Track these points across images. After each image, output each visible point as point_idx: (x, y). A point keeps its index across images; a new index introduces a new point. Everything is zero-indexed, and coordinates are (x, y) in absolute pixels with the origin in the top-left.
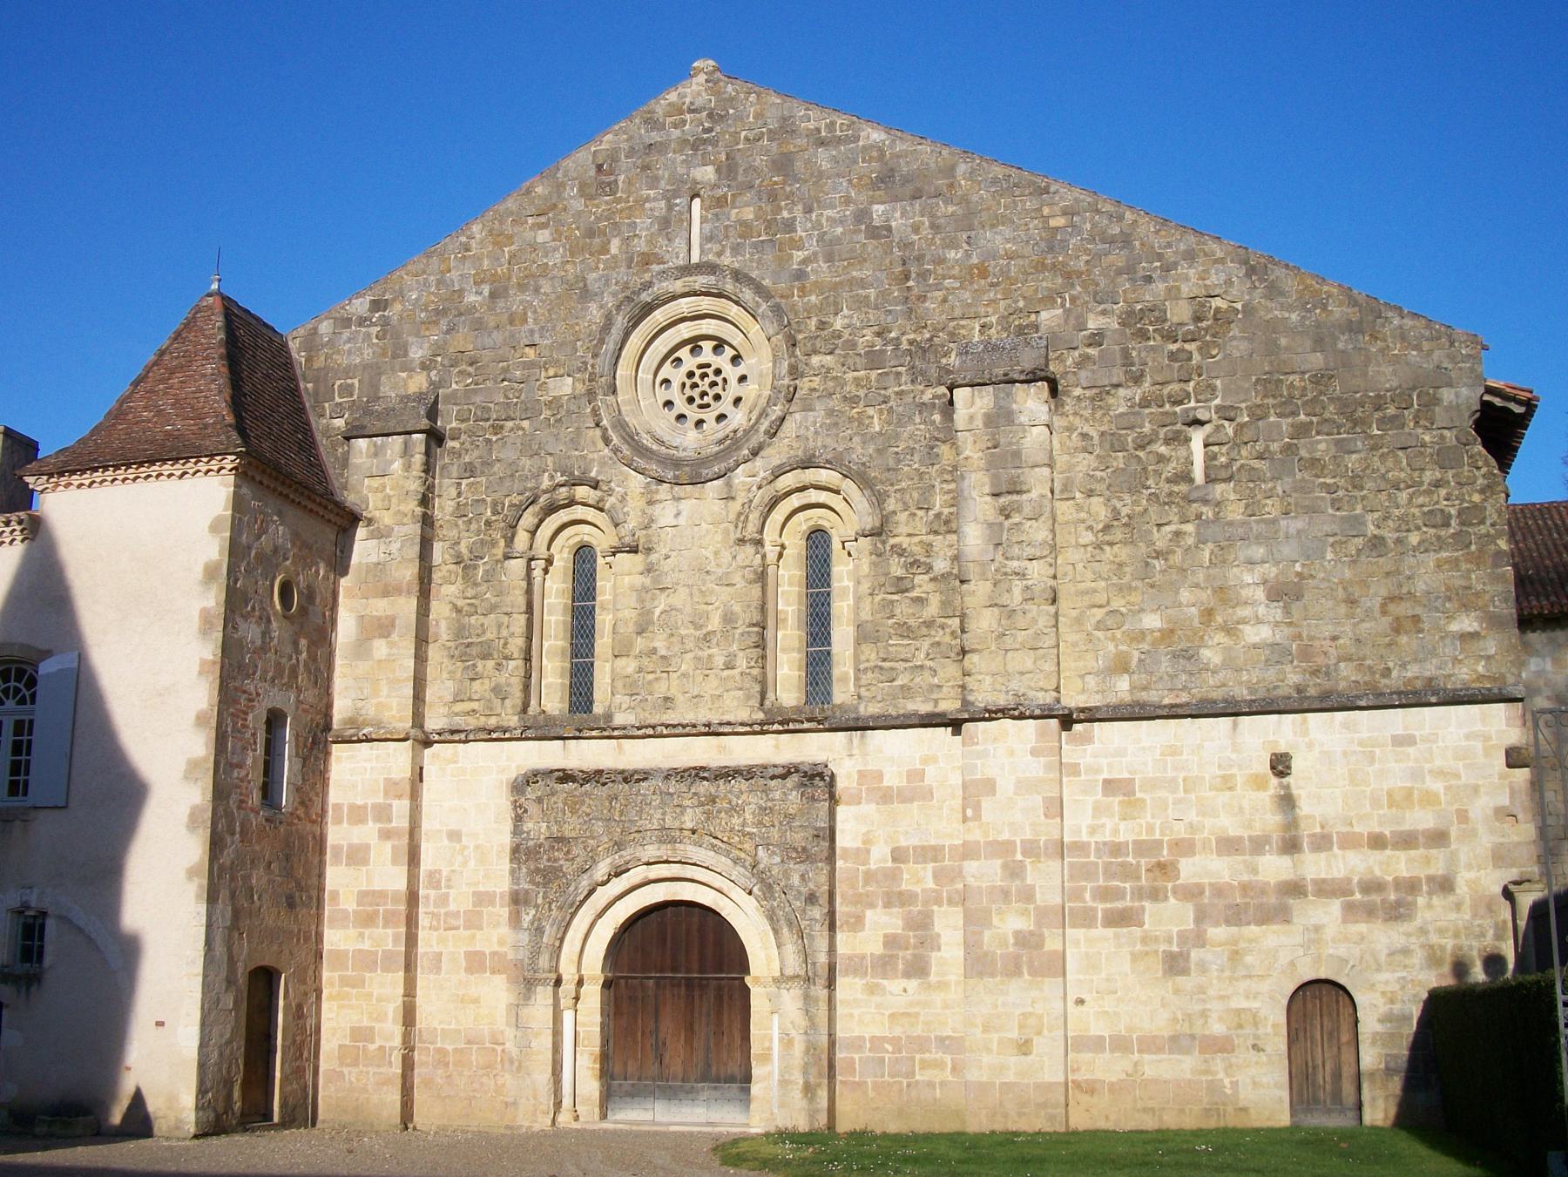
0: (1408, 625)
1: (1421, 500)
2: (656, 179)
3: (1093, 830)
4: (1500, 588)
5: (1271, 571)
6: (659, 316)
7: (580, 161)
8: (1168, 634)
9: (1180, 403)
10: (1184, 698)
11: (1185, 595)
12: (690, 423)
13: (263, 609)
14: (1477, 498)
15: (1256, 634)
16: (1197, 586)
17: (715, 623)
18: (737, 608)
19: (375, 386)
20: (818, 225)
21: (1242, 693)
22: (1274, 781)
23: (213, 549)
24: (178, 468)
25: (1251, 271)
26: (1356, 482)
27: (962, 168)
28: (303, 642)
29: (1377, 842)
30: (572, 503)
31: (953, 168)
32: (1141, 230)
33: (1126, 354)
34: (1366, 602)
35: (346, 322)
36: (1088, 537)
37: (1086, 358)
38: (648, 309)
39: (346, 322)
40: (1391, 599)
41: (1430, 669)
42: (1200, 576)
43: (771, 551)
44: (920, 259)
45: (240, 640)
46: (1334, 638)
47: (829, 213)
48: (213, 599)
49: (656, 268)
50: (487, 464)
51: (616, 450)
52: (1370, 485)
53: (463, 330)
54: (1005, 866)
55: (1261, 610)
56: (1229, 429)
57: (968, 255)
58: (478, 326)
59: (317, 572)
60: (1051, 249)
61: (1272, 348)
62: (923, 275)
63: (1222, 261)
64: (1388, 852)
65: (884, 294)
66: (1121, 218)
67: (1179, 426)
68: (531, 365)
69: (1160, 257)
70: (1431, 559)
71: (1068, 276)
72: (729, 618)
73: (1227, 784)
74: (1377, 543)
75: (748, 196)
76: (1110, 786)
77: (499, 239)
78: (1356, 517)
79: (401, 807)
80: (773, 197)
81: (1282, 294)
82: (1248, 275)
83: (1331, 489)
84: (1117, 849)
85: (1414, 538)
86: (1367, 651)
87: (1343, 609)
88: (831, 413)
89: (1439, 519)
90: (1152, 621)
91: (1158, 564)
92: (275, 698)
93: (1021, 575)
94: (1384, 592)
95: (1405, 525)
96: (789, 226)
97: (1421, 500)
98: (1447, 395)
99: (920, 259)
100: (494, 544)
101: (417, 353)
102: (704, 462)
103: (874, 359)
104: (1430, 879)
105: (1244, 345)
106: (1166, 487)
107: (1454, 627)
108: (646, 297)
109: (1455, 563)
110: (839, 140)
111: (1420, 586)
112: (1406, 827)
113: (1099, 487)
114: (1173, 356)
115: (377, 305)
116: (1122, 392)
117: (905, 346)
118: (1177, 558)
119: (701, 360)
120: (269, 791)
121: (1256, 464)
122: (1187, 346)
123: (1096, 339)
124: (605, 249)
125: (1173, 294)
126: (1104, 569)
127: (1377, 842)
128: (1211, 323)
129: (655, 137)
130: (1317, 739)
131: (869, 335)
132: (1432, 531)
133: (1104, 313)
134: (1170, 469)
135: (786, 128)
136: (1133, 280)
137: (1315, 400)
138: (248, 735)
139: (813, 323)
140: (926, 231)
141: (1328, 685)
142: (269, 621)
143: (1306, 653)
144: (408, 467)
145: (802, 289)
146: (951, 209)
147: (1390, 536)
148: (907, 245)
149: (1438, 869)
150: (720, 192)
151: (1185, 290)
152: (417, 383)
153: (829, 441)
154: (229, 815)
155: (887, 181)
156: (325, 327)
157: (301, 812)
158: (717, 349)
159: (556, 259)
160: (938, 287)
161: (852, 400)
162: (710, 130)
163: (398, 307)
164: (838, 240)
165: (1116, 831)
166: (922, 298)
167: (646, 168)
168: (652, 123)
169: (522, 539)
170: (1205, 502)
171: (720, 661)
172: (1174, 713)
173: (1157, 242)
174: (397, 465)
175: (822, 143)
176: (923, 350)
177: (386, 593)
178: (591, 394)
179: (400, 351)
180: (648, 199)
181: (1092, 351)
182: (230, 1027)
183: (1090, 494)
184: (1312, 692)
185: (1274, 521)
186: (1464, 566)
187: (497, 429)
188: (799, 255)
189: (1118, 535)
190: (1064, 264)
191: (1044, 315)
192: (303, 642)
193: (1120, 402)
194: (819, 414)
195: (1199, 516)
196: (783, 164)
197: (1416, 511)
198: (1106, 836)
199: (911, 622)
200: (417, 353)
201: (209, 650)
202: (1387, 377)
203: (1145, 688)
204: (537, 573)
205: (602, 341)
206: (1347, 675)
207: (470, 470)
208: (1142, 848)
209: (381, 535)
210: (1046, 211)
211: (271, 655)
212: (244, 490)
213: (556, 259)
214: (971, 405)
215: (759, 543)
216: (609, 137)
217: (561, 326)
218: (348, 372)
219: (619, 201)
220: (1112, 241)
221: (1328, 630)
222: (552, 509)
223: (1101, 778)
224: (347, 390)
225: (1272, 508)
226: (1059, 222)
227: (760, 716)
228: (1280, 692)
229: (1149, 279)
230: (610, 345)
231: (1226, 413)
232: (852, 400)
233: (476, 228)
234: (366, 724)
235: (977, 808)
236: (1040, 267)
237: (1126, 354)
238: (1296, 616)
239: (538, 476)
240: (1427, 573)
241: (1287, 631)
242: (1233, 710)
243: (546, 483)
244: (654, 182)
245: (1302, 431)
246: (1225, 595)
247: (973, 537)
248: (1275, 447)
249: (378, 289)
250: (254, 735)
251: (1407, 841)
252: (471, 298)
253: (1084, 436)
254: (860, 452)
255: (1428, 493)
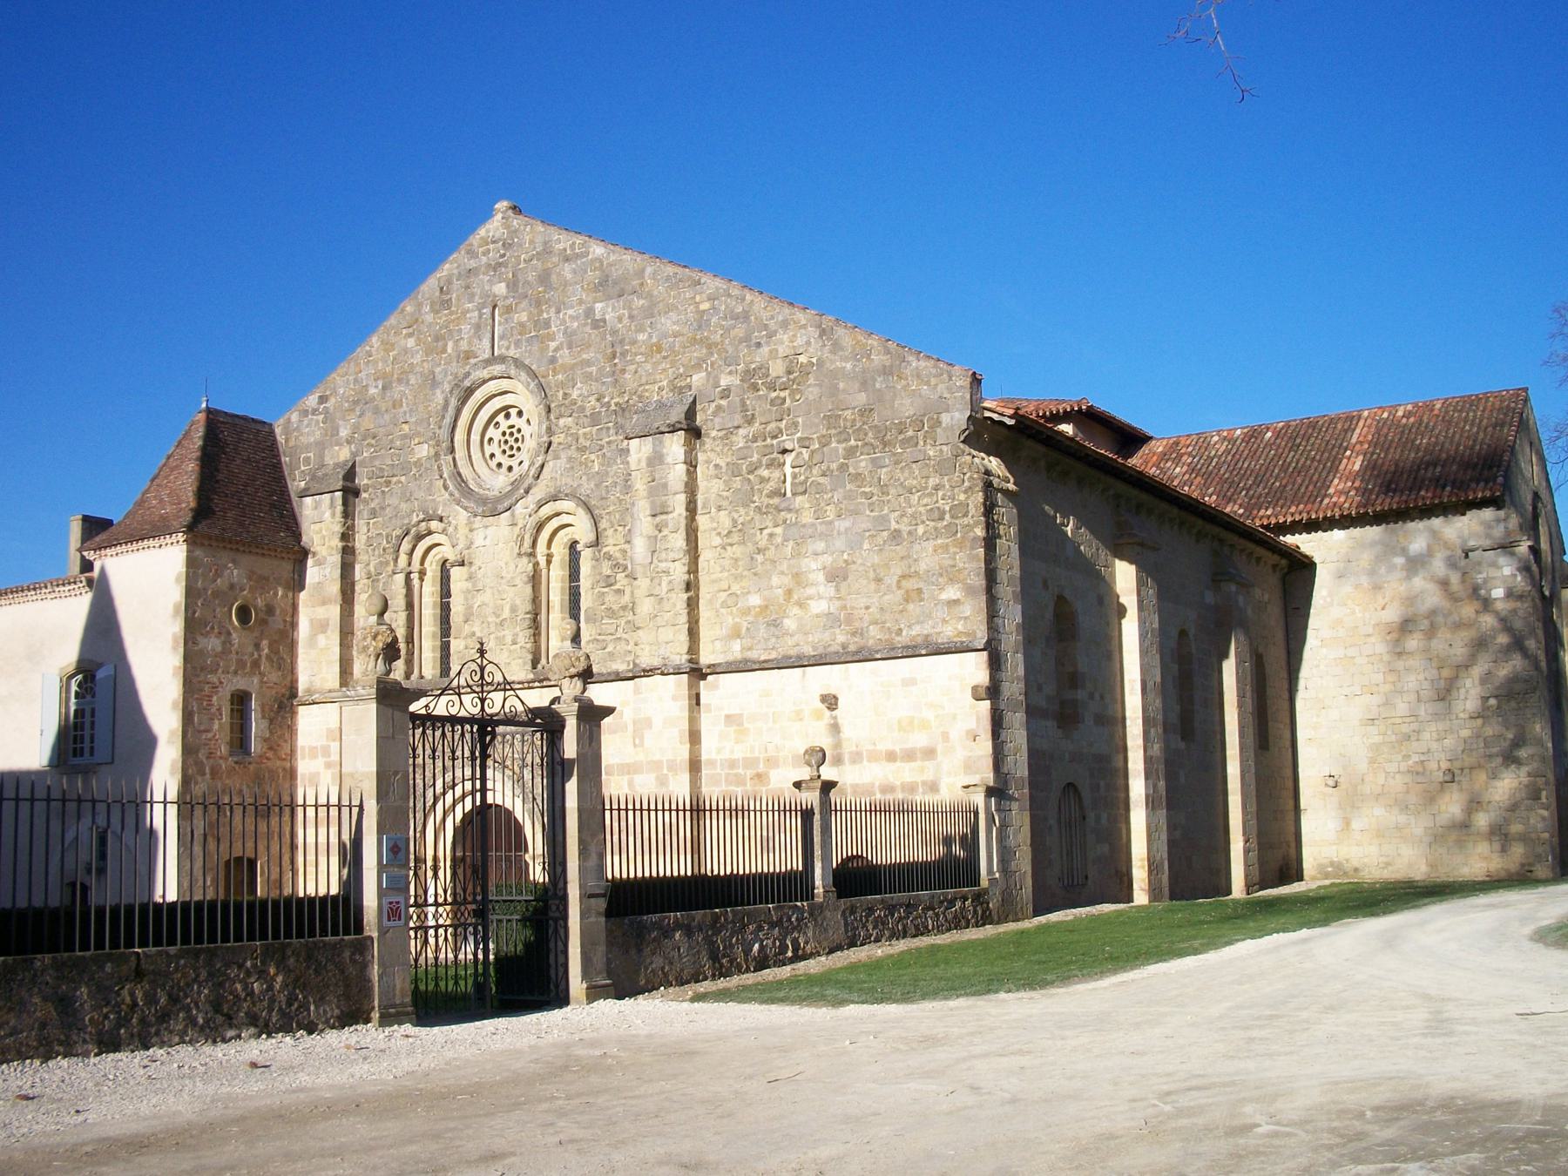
0: (914, 595)
1: (925, 501)
2: (473, 295)
3: (719, 751)
4: (974, 565)
5: (827, 560)
6: (479, 395)
7: (430, 285)
8: (764, 608)
9: (775, 437)
10: (773, 655)
11: (775, 580)
12: (504, 469)
13: (221, 626)
14: (962, 497)
15: (819, 607)
16: (782, 573)
17: (506, 613)
18: (518, 602)
19: (322, 457)
20: (563, 322)
21: (808, 650)
22: (827, 713)
23: (176, 594)
24: (156, 542)
25: (823, 332)
26: (884, 490)
27: (649, 270)
28: (265, 643)
29: (891, 757)
30: (430, 533)
31: (643, 271)
32: (755, 308)
33: (743, 403)
34: (887, 580)
35: (305, 413)
36: (717, 541)
37: (719, 408)
38: (470, 392)
39: (305, 413)
40: (903, 577)
41: (927, 629)
42: (784, 567)
43: (542, 561)
44: (622, 342)
45: (201, 651)
46: (867, 608)
47: (570, 312)
48: (177, 627)
49: (473, 361)
50: (383, 508)
51: (451, 495)
52: (893, 491)
53: (369, 414)
54: (657, 778)
55: (822, 589)
56: (806, 454)
57: (650, 337)
58: (377, 411)
59: (276, 594)
60: (700, 327)
61: (834, 391)
62: (624, 354)
63: (804, 327)
64: (898, 764)
65: (600, 370)
66: (743, 299)
67: (775, 455)
68: (405, 437)
69: (766, 327)
70: (929, 546)
71: (709, 347)
72: (513, 609)
73: (799, 716)
74: (896, 535)
75: (524, 304)
76: (729, 719)
77: (388, 346)
78: (883, 517)
79: (335, 746)
80: (538, 303)
81: (842, 349)
82: (820, 336)
83: (869, 496)
84: (732, 764)
85: (921, 529)
86: (887, 616)
87: (873, 586)
88: (570, 459)
89: (936, 515)
90: (755, 600)
91: (760, 558)
92: (240, 683)
93: (667, 572)
94: (899, 572)
95: (915, 519)
96: (547, 324)
97: (925, 501)
98: (945, 418)
99: (622, 342)
100: (387, 563)
101: (344, 433)
102: (499, 500)
103: (595, 419)
104: (924, 783)
105: (816, 390)
106: (766, 501)
107: (944, 596)
108: (467, 383)
109: (945, 547)
110: (578, 256)
111: (923, 566)
112: (909, 745)
113: (725, 503)
114: (772, 402)
115: (323, 399)
116: (741, 432)
117: (613, 407)
118: (771, 553)
119: (510, 422)
120: (240, 741)
121: (822, 480)
122: (782, 394)
123: (726, 393)
124: (444, 351)
125: (773, 354)
126: (727, 563)
127: (891, 757)
128: (796, 374)
129: (473, 264)
130: (853, 682)
131: (592, 399)
132: (932, 524)
133: (730, 373)
134: (771, 486)
135: (547, 251)
136: (749, 347)
137: (859, 429)
138: (214, 710)
139: (560, 394)
140: (626, 321)
141: (862, 642)
142: (229, 634)
143: (849, 619)
144: (333, 515)
145: (554, 370)
146: (642, 302)
147: (904, 528)
148: (614, 332)
149: (929, 776)
150: (508, 302)
151: (781, 352)
152: (344, 454)
153: (569, 481)
154: (200, 766)
155: (608, 286)
156: (295, 417)
157: (270, 754)
158: (508, 416)
159: (417, 359)
160: (632, 362)
161: (582, 450)
162: (503, 256)
163: (332, 400)
164: (574, 333)
165: (732, 752)
166: (623, 371)
167: (467, 287)
168: (472, 254)
169: (403, 559)
170: (789, 510)
171: (509, 639)
172: (764, 666)
173: (765, 315)
174: (328, 514)
175: (567, 260)
176: (623, 409)
177: (324, 603)
178: (437, 455)
179: (335, 431)
180: (468, 311)
181: (723, 402)
182: (1278, 728)
183: (719, 508)
184: (852, 648)
185: (831, 523)
186: (952, 550)
187: (388, 483)
188: (553, 345)
189: (735, 538)
190: (707, 338)
191: (695, 378)
192: (265, 643)
193: (739, 440)
194: (562, 462)
195: (785, 521)
196: (544, 278)
197: (922, 509)
198: (726, 755)
199: (615, 607)
200: (344, 433)
201: (176, 660)
202: (906, 407)
203: (750, 649)
204: (416, 582)
205: (443, 417)
206: (874, 635)
207: (374, 514)
208: (749, 762)
209: (319, 563)
210: (698, 298)
211: (234, 656)
212: (198, 553)
213: (417, 359)
214: (639, 450)
215: (532, 555)
216: (447, 266)
217: (421, 408)
218: (308, 448)
219: (452, 313)
220: (736, 317)
221: (862, 602)
222: (419, 538)
223: (723, 713)
224: (307, 460)
225: (831, 512)
226: (705, 306)
227: (531, 676)
228: (832, 649)
229: (759, 345)
230: (448, 420)
231: (804, 443)
232: (582, 450)
233: (374, 339)
234: (315, 692)
235: (642, 739)
236: (694, 341)
237: (743, 403)
238: (843, 592)
239: (409, 515)
240: (927, 557)
241: (838, 603)
242: (800, 662)
243: (415, 519)
244: (471, 299)
245: (851, 453)
246: (798, 578)
247: (640, 547)
248: (834, 466)
249: (322, 387)
250: (219, 709)
251: (909, 756)
252: (372, 391)
253: (716, 466)
254: (586, 487)
255: (930, 495)
